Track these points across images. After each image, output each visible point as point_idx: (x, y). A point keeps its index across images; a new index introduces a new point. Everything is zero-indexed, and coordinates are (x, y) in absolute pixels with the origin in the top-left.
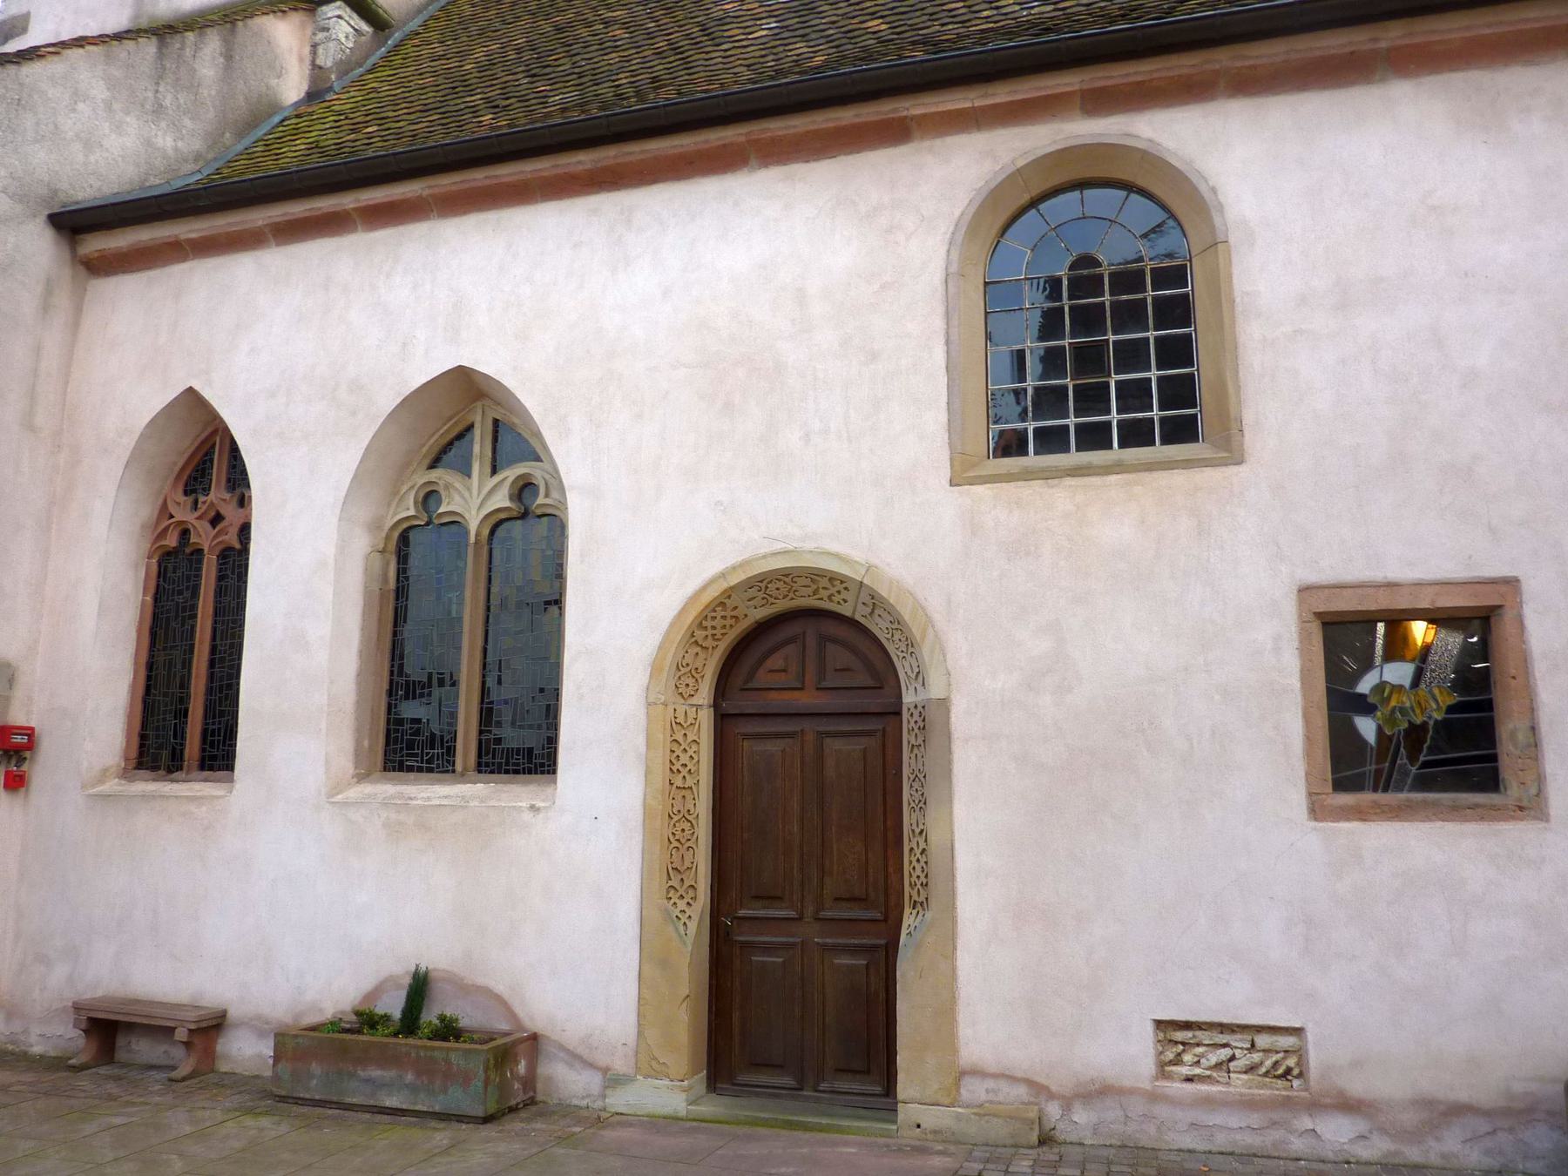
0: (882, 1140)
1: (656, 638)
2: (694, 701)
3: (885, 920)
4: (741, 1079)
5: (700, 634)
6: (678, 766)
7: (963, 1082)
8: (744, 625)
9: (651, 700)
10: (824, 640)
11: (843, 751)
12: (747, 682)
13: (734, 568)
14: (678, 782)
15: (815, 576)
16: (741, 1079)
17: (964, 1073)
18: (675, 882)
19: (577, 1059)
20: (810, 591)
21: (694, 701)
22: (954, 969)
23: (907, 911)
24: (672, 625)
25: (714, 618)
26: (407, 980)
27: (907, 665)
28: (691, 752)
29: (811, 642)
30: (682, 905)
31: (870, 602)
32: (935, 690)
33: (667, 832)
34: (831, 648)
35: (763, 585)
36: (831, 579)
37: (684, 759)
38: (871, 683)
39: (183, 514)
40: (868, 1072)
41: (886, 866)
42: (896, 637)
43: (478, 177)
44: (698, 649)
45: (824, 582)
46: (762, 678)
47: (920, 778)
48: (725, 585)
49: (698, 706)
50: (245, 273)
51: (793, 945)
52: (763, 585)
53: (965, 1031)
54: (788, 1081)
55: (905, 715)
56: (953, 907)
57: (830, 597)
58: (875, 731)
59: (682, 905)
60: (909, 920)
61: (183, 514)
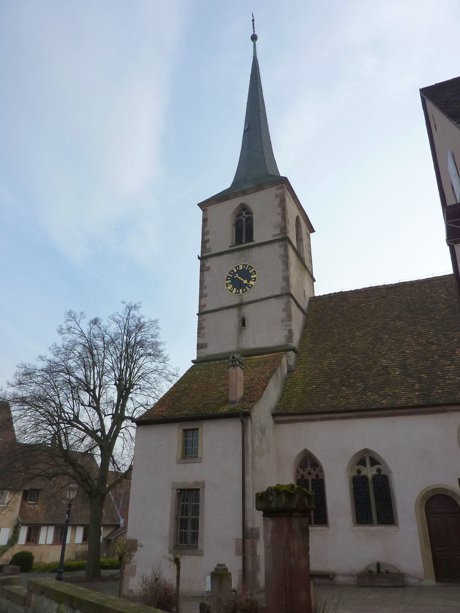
15: (442, 489)
19: (414, 577)
26: (376, 564)
39: (301, 472)
43: (365, 413)
50: (313, 426)
61: (301, 472)
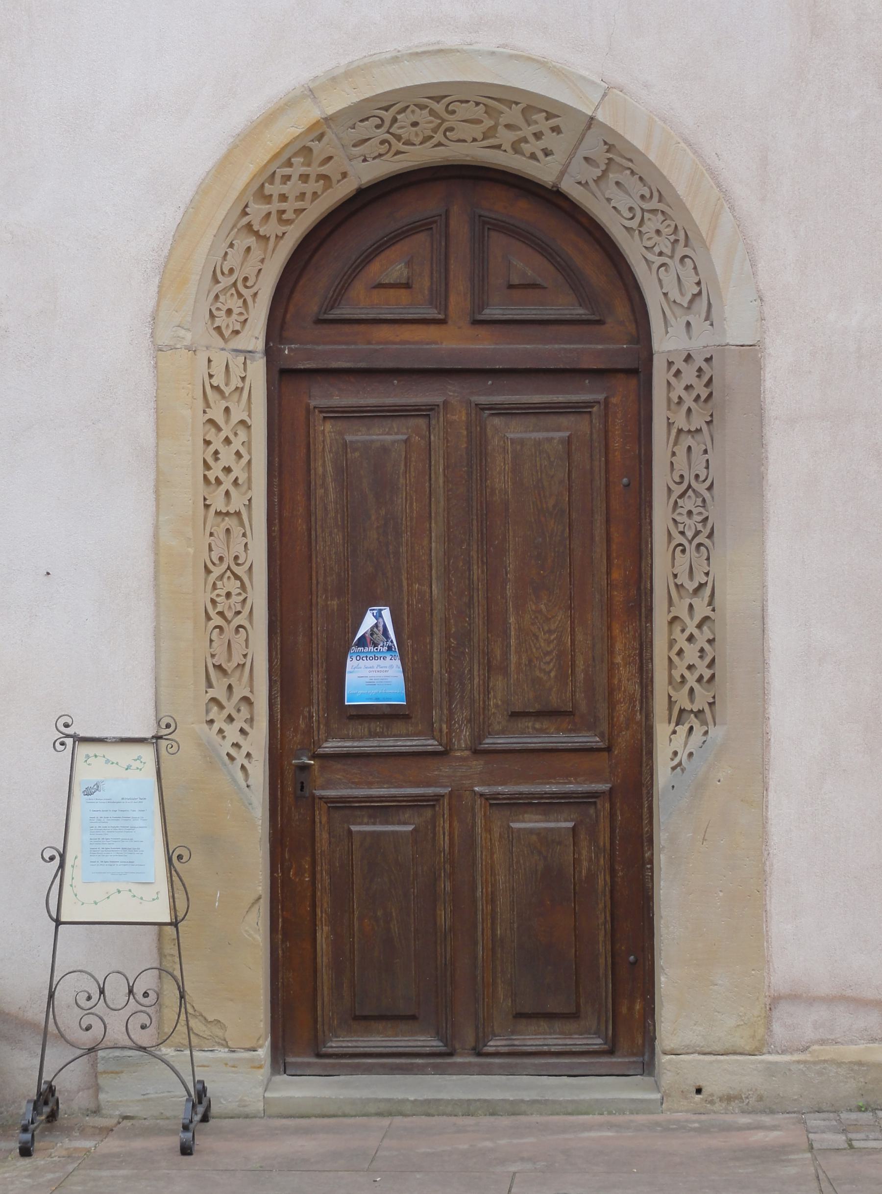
0: (641, 1118)
1: (168, 217)
2: (240, 343)
3: (609, 749)
4: (334, 1045)
5: (258, 209)
6: (216, 471)
7: (776, 1014)
8: (342, 191)
9: (164, 339)
10: (485, 226)
11: (529, 443)
12: (334, 303)
13: (334, 80)
14: (219, 503)
16: (334, 1045)
17: (775, 1001)
18: (218, 691)
20: (477, 131)
21: (240, 343)
22: (764, 823)
23: (662, 729)
24: (203, 190)
25: (287, 178)
27: (669, 280)
28: (236, 445)
29: (460, 227)
30: (232, 732)
31: (601, 157)
32: (736, 328)
33: (204, 598)
34: (498, 242)
35: (388, 116)
36: (528, 111)
37: (227, 457)
38: (580, 312)
40: (574, 1016)
41: (611, 652)
42: (650, 226)
44: (251, 241)
45: (513, 115)
46: (361, 301)
47: (696, 489)
48: (315, 114)
49: (248, 353)
51: (438, 798)
52: (388, 116)
53: (781, 926)
54: (428, 1042)
55: (660, 375)
56: (765, 719)
57: (516, 148)
58: (589, 404)
59: (232, 732)
60: (667, 742)
